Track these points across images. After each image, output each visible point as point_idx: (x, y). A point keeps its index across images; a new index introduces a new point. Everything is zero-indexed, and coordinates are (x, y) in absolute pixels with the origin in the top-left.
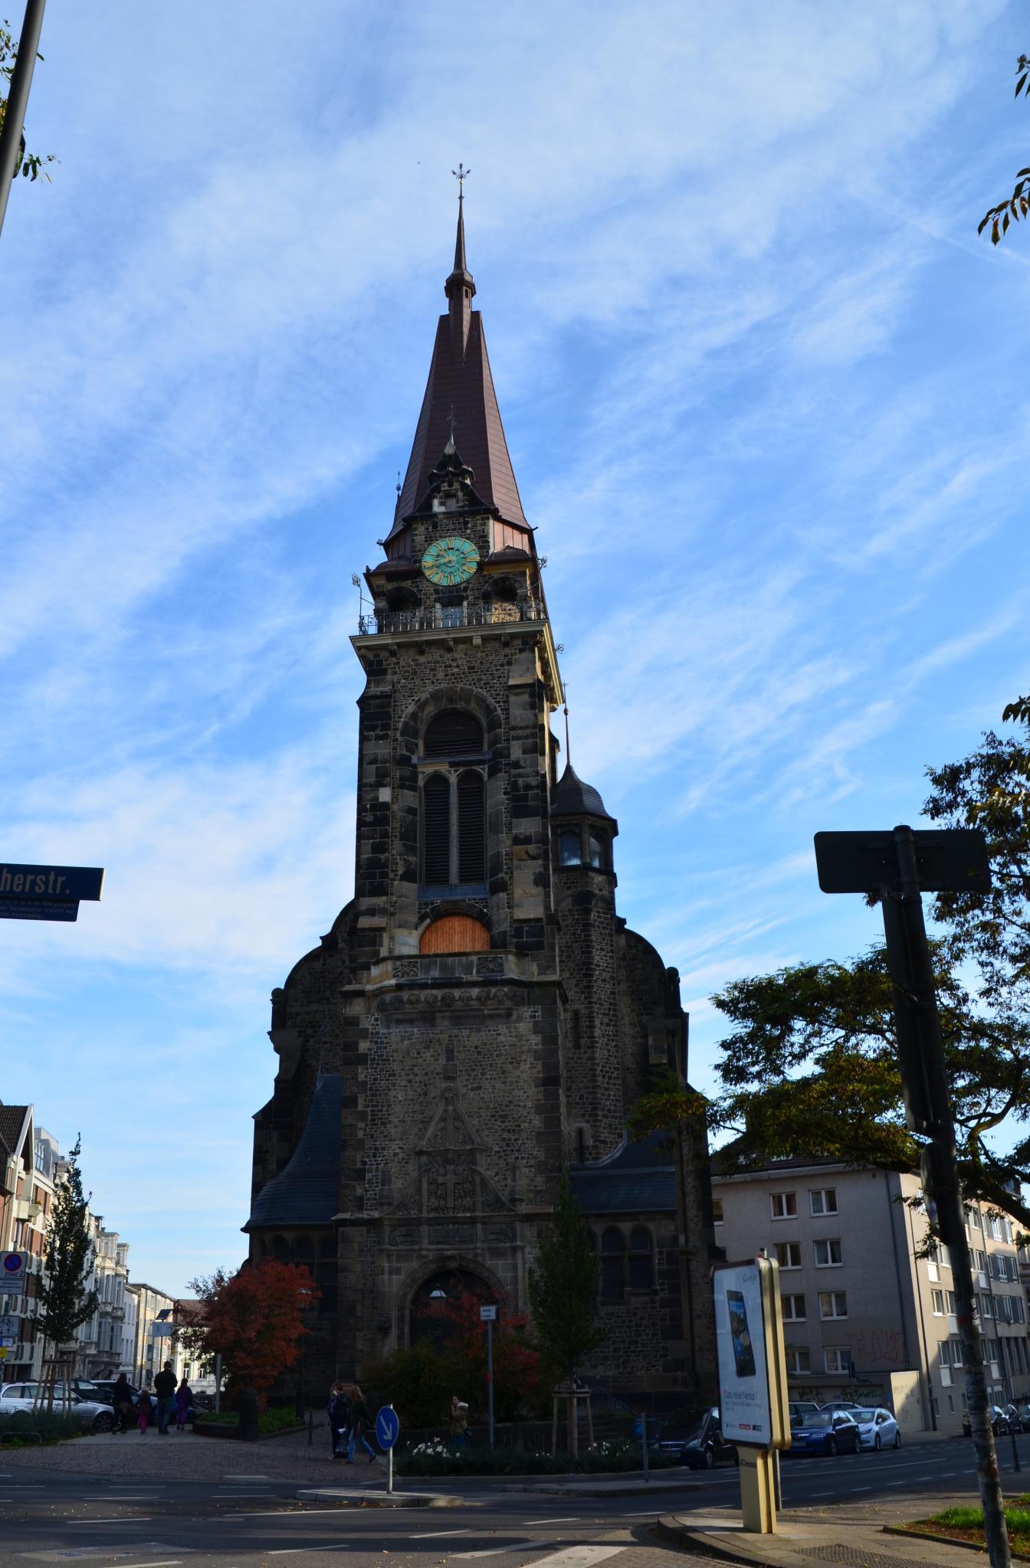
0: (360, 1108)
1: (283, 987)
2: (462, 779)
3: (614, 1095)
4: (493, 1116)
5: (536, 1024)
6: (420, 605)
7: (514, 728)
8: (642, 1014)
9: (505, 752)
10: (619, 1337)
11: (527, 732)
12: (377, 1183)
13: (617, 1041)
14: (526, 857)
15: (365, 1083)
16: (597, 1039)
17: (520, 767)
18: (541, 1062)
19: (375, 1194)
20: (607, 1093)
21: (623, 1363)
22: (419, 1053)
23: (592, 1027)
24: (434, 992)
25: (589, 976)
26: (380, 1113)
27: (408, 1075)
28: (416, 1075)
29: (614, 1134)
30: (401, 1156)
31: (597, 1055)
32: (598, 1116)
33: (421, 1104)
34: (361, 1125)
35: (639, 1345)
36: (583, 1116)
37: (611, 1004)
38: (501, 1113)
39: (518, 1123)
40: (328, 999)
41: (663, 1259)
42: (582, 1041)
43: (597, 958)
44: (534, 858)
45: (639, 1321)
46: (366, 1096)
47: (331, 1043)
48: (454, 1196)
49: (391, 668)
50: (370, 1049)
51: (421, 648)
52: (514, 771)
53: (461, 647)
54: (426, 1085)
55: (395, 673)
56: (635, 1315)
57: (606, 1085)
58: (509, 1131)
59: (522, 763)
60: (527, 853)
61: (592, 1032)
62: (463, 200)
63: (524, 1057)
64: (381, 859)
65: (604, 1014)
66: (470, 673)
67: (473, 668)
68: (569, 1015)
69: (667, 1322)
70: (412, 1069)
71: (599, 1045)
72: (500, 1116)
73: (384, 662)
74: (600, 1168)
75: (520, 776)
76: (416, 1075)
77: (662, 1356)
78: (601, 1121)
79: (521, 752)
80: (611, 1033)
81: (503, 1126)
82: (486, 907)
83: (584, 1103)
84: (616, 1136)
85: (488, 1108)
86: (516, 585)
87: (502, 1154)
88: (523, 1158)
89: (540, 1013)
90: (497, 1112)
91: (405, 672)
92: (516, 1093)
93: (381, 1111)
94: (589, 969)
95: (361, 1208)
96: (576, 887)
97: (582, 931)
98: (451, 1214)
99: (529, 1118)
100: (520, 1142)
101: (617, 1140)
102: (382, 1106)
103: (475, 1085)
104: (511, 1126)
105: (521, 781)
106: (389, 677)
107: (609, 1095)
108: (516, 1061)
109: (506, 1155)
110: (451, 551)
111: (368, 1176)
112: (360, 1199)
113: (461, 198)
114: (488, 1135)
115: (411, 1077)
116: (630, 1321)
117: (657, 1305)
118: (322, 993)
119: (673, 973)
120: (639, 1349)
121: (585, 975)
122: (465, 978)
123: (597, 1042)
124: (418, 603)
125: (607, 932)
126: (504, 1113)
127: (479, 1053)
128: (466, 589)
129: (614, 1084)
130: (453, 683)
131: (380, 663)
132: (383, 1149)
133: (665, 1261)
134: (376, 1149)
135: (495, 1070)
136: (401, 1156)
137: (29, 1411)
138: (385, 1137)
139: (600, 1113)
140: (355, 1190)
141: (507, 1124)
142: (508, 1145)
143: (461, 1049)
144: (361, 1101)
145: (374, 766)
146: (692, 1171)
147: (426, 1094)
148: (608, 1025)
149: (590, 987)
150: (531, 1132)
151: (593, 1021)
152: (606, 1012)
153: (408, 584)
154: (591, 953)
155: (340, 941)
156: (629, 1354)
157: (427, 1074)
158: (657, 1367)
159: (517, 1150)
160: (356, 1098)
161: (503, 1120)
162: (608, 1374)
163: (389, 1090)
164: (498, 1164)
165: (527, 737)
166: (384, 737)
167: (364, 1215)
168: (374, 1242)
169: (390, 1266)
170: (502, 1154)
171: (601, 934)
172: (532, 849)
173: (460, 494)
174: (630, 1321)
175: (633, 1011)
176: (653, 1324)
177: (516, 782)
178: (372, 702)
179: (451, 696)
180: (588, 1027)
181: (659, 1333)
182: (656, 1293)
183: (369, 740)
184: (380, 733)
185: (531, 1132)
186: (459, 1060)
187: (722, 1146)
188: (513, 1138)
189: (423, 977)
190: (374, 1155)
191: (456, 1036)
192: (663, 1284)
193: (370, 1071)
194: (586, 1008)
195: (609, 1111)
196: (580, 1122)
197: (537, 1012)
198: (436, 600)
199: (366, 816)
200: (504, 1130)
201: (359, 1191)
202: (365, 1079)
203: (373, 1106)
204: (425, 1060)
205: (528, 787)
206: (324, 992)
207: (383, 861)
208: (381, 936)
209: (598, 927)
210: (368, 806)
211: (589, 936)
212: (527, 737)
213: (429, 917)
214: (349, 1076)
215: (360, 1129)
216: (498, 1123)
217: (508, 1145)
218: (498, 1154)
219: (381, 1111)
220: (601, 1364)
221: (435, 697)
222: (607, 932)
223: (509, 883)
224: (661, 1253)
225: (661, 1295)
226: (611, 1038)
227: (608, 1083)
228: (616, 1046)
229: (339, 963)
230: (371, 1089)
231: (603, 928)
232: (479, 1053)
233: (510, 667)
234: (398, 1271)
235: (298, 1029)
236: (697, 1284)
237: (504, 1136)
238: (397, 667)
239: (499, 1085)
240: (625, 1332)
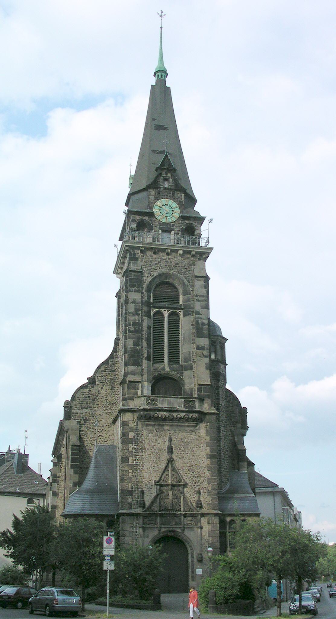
1: (70, 400)
2: (170, 315)
5: (207, 431)
6: (153, 230)
7: (197, 296)
8: (231, 427)
9: (192, 306)
11: (202, 299)
14: (202, 356)
17: (199, 314)
18: (209, 448)
22: (156, 440)
24: (165, 413)
26: (139, 466)
30: (148, 486)
32: (221, 471)
33: (157, 463)
38: (192, 469)
39: (199, 474)
40: (92, 407)
43: (221, 402)
44: (206, 357)
46: (133, 458)
47: (93, 428)
49: (140, 258)
51: (156, 251)
52: (197, 316)
53: (174, 254)
55: (142, 261)
58: (195, 477)
59: (200, 312)
62: (162, 29)
64: (137, 349)
66: (176, 266)
67: (178, 264)
72: (192, 470)
73: (137, 255)
74: (223, 493)
75: (201, 318)
79: (200, 307)
86: (196, 228)
87: (193, 487)
91: (147, 261)
93: (139, 465)
95: (131, 508)
98: (175, 512)
104: (196, 475)
105: (200, 321)
106: (139, 262)
110: (166, 206)
112: (130, 504)
113: (161, 27)
115: (153, 450)
118: (88, 404)
119: (245, 410)
122: (180, 409)
124: (151, 228)
126: (193, 469)
128: (173, 225)
130: (169, 270)
131: (135, 254)
136: (148, 486)
137: (85, 608)
140: (128, 500)
142: (195, 483)
144: (130, 459)
145: (134, 304)
150: (205, 478)
153: (146, 218)
155: (97, 381)
161: (193, 472)
165: (203, 301)
166: (138, 291)
167: (133, 511)
173: (171, 180)
177: (198, 321)
178: (133, 273)
179: (166, 275)
183: (132, 292)
184: (136, 289)
185: (205, 478)
186: (174, 444)
189: (160, 406)
193: (134, 446)
198: (160, 228)
199: (130, 328)
201: (130, 500)
202: (132, 450)
204: (159, 443)
205: (203, 324)
206: (90, 404)
207: (138, 350)
208: (138, 385)
210: (131, 323)
212: (203, 301)
214: (125, 449)
215: (130, 472)
216: (191, 473)
217: (195, 483)
218: (191, 487)
219: (139, 465)
221: (160, 275)
223: (194, 367)
229: (97, 391)
232: (183, 442)
233: (195, 267)
235: (77, 421)
237: (193, 479)
238: (143, 258)
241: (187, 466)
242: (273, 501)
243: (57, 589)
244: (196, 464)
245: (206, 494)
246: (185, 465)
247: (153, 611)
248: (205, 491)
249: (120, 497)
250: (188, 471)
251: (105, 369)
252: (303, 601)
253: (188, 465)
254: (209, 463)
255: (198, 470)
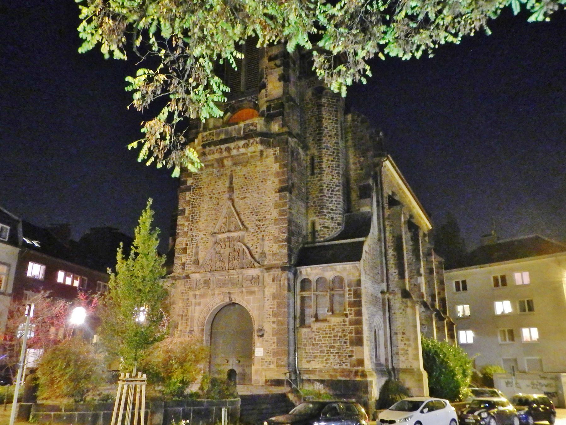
0: (186, 214)
3: (336, 201)
4: (251, 213)
5: (276, 158)
10: (324, 343)
12: (192, 255)
13: (338, 170)
15: (189, 201)
16: (324, 169)
19: (191, 261)
20: (330, 200)
21: (326, 360)
23: (321, 162)
25: (320, 134)
26: (195, 217)
27: (210, 194)
28: (214, 194)
29: (335, 223)
30: (204, 239)
31: (324, 178)
34: (186, 224)
35: (336, 349)
36: (315, 213)
37: (334, 149)
38: (256, 210)
41: (351, 294)
42: (316, 171)
44: (278, 66)
45: (336, 334)
48: (229, 260)
50: (192, 183)
54: (218, 199)
56: (333, 329)
57: (329, 195)
60: (276, 64)
61: (321, 165)
63: (269, 178)
65: (330, 155)
68: (308, 158)
69: (353, 335)
70: (212, 191)
71: (325, 172)
72: (255, 212)
76: (214, 194)
77: (350, 356)
78: (326, 215)
80: (334, 166)
81: (257, 218)
82: (256, 100)
83: (316, 206)
84: (336, 224)
85: (249, 208)
88: (266, 235)
89: (278, 151)
90: (254, 210)
92: (265, 198)
93: (196, 215)
94: (320, 130)
96: (313, 86)
97: (317, 109)
99: (271, 212)
100: (265, 226)
101: (337, 227)
102: (197, 213)
103: (243, 197)
107: (332, 201)
108: (264, 180)
109: (258, 234)
111: (188, 251)
114: (248, 224)
116: (331, 333)
117: (347, 323)
120: (336, 351)
121: (318, 134)
123: (324, 171)
125: (333, 109)
127: (246, 178)
129: (336, 195)
132: (196, 236)
133: (352, 296)
134: (193, 236)
135: (253, 187)
136: (204, 239)
138: (197, 230)
139: (325, 211)
141: (258, 216)
142: (259, 228)
143: (237, 177)
146: (392, 246)
147: (218, 204)
148: (332, 161)
149: (320, 140)
151: (322, 159)
152: (332, 154)
154: (322, 121)
156: (330, 354)
157: (219, 193)
158: (346, 364)
159: (264, 231)
160: (185, 209)
162: (316, 367)
163: (200, 204)
164: (253, 240)
168: (189, 288)
169: (195, 301)
170: (256, 234)
171: (329, 110)
172: (278, 62)
174: (331, 333)
175: (355, 155)
176: (345, 336)
180: (319, 162)
181: (348, 341)
182: (346, 315)
187: (86, 50)
188: (262, 224)
190: (192, 240)
191: (235, 170)
192: (351, 310)
194: (318, 152)
195: (332, 210)
196: (313, 217)
197: (276, 151)
200: (257, 220)
203: (193, 213)
209: (327, 107)
211: (321, 111)
213: (229, 111)
216: (254, 216)
217: (259, 228)
220: (312, 360)
222: (333, 109)
224: (350, 290)
225: (350, 317)
226: (334, 168)
227: (331, 194)
228: (337, 173)
230: (192, 204)
231: (331, 107)
234: (199, 304)
236: (394, 313)
237: (257, 223)
239: (255, 195)
240: (327, 340)
241: (249, 208)
242: (532, 335)
243: (461, 403)
244: (261, 204)
245: (271, 241)
246: (247, 207)
247: (380, 393)
248: (271, 237)
249: (412, 337)
250: (250, 214)
251: (323, 199)
252: (399, 366)
253: (251, 207)
254: (277, 199)
255: (263, 212)
